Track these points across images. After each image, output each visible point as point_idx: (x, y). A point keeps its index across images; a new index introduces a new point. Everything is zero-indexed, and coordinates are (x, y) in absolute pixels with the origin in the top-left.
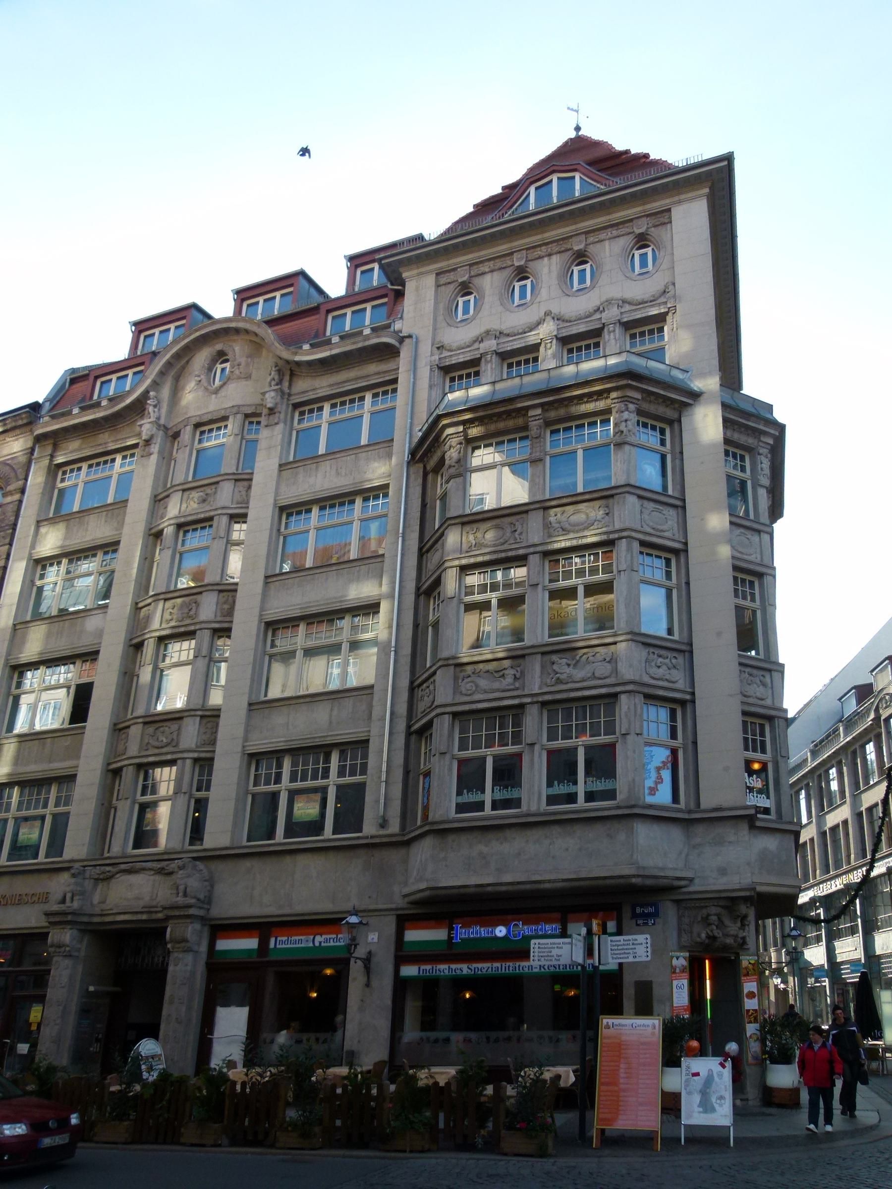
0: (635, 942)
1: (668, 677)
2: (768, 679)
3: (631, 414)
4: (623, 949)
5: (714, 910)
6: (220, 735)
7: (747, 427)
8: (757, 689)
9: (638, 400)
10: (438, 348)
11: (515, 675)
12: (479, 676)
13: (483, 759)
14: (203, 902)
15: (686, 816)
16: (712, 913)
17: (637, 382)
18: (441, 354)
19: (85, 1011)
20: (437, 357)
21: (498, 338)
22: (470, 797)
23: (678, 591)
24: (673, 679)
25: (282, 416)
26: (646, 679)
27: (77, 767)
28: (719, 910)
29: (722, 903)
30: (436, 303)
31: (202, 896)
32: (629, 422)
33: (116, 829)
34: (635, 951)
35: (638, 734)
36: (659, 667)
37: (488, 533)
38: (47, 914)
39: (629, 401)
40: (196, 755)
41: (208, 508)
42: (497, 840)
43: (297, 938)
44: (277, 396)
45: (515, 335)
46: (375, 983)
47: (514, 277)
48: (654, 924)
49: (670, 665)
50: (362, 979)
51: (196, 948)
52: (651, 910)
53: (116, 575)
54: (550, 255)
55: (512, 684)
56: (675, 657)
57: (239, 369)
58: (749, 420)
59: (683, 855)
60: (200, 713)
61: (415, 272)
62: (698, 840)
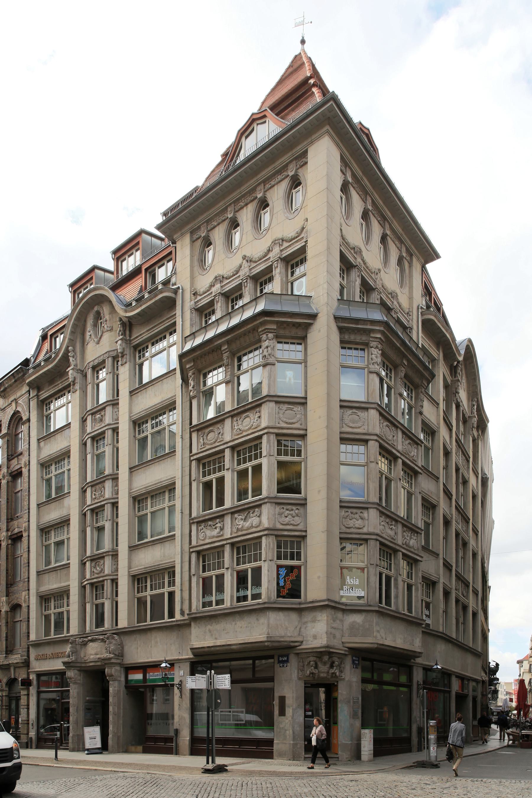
5: (312, 659)
6: (119, 567)
7: (359, 330)
8: (357, 522)
9: (275, 329)
10: (194, 294)
11: (220, 527)
14: (118, 656)
18: (196, 298)
19: (88, 709)
20: (193, 302)
21: (222, 282)
22: (242, 593)
24: (295, 524)
25: (128, 357)
27: (69, 585)
28: (315, 659)
30: (192, 256)
31: (117, 653)
32: (269, 348)
35: (271, 560)
36: (286, 517)
37: (210, 434)
39: (268, 332)
40: (111, 577)
41: (103, 425)
42: (215, 622)
43: (156, 673)
44: (123, 343)
45: (230, 278)
46: (183, 696)
47: (231, 227)
48: (286, 666)
50: (179, 694)
51: (119, 679)
52: (286, 659)
53: (71, 471)
54: (247, 205)
56: (297, 509)
57: (106, 324)
59: (298, 628)
60: (110, 553)
61: (179, 234)
62: (305, 620)
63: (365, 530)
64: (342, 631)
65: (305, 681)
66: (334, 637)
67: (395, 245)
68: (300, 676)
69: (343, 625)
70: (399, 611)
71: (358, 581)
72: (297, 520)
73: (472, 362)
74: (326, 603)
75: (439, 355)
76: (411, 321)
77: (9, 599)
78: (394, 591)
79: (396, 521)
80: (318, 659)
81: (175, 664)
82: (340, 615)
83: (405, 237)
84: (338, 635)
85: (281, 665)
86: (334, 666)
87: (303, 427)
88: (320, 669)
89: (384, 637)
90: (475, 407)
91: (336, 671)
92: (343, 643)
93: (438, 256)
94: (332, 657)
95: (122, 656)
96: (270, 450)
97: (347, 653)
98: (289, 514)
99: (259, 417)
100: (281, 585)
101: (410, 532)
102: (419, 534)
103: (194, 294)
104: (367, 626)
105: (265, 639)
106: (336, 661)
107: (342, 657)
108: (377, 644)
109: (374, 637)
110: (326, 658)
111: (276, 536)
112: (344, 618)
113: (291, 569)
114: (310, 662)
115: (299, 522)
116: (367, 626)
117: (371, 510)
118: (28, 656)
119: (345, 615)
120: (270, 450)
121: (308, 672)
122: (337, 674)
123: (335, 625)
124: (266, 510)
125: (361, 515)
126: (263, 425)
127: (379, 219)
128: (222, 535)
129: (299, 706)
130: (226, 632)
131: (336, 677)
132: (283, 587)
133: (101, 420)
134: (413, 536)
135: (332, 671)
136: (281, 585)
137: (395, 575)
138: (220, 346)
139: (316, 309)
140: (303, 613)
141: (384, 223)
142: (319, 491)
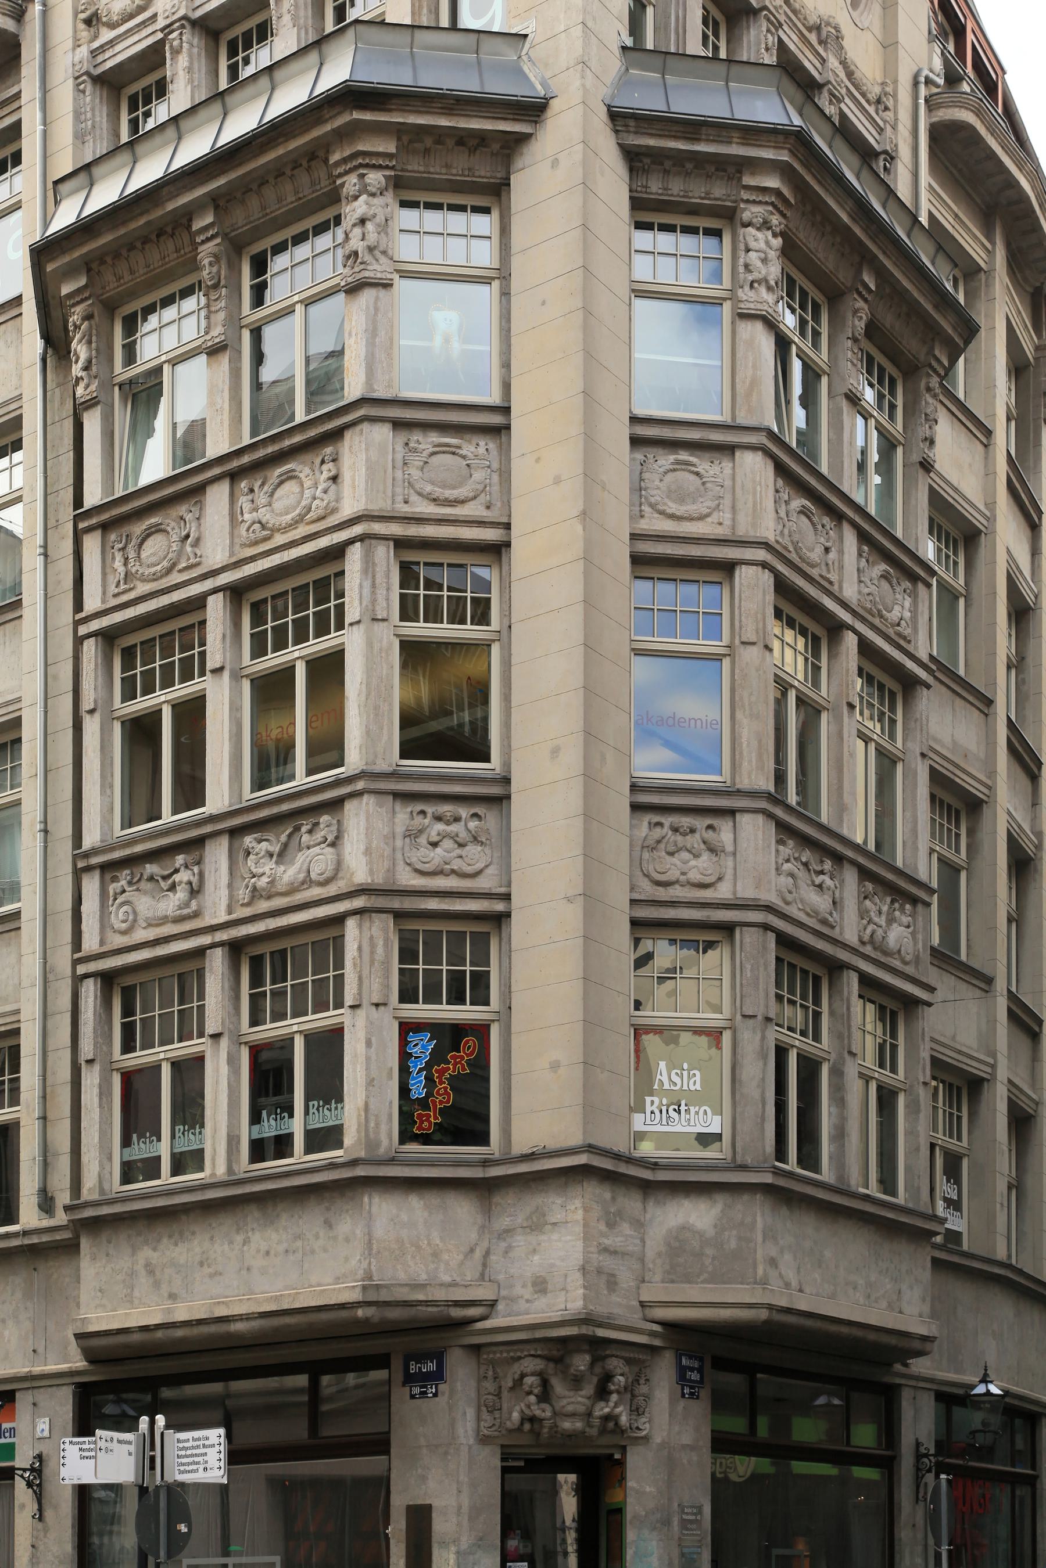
0: (207, 1443)
1: (456, 865)
3: (378, 201)
4: (192, 1456)
5: (531, 1365)
9: (389, 156)
10: (88, 22)
12: (138, 890)
13: (287, 1043)
15: (477, 1173)
16: (528, 1370)
17: (373, 109)
18: (96, 37)
20: (84, 51)
22: (269, 1128)
23: (502, 648)
26: (408, 879)
32: (370, 226)
34: (206, 1458)
35: (377, 1005)
42: (170, 1237)
46: (48, 1514)
48: (435, 1395)
49: (463, 835)
50: (32, 1507)
52: (431, 1366)
55: (187, 905)
56: (475, 815)
58: (697, 140)
59: (478, 1254)
62: (505, 1222)
63: (723, 892)
64: (642, 1260)
65: (502, 1446)
66: (612, 1283)
68: (486, 1432)
69: (643, 1241)
70: (849, 1186)
71: (698, 1078)
76: (889, 129)
78: (830, 1113)
80: (551, 1365)
81: (18, 1395)
82: (631, 1203)
84: (626, 1278)
85: (416, 1390)
86: (611, 1393)
89: (794, 1284)
91: (618, 1410)
92: (643, 1305)
94: (604, 1358)
96: (374, 601)
97: (657, 1342)
98: (443, 836)
99: (334, 479)
100: (414, 1095)
103: (88, 22)
104: (733, 1244)
106: (619, 1371)
108: (770, 1307)
109: (755, 1283)
110: (581, 1362)
111: (399, 915)
112: (648, 1216)
115: (480, 866)
116: (733, 1244)
119: (651, 1204)
120: (374, 601)
121: (516, 1415)
122: (624, 1419)
125: (710, 835)
128: (196, 915)
129: (481, 1539)
130: (211, 1270)
131: (619, 1430)
132: (423, 1103)
134: (897, 913)
135: (602, 1409)
138: (187, 214)
142: (555, 751)
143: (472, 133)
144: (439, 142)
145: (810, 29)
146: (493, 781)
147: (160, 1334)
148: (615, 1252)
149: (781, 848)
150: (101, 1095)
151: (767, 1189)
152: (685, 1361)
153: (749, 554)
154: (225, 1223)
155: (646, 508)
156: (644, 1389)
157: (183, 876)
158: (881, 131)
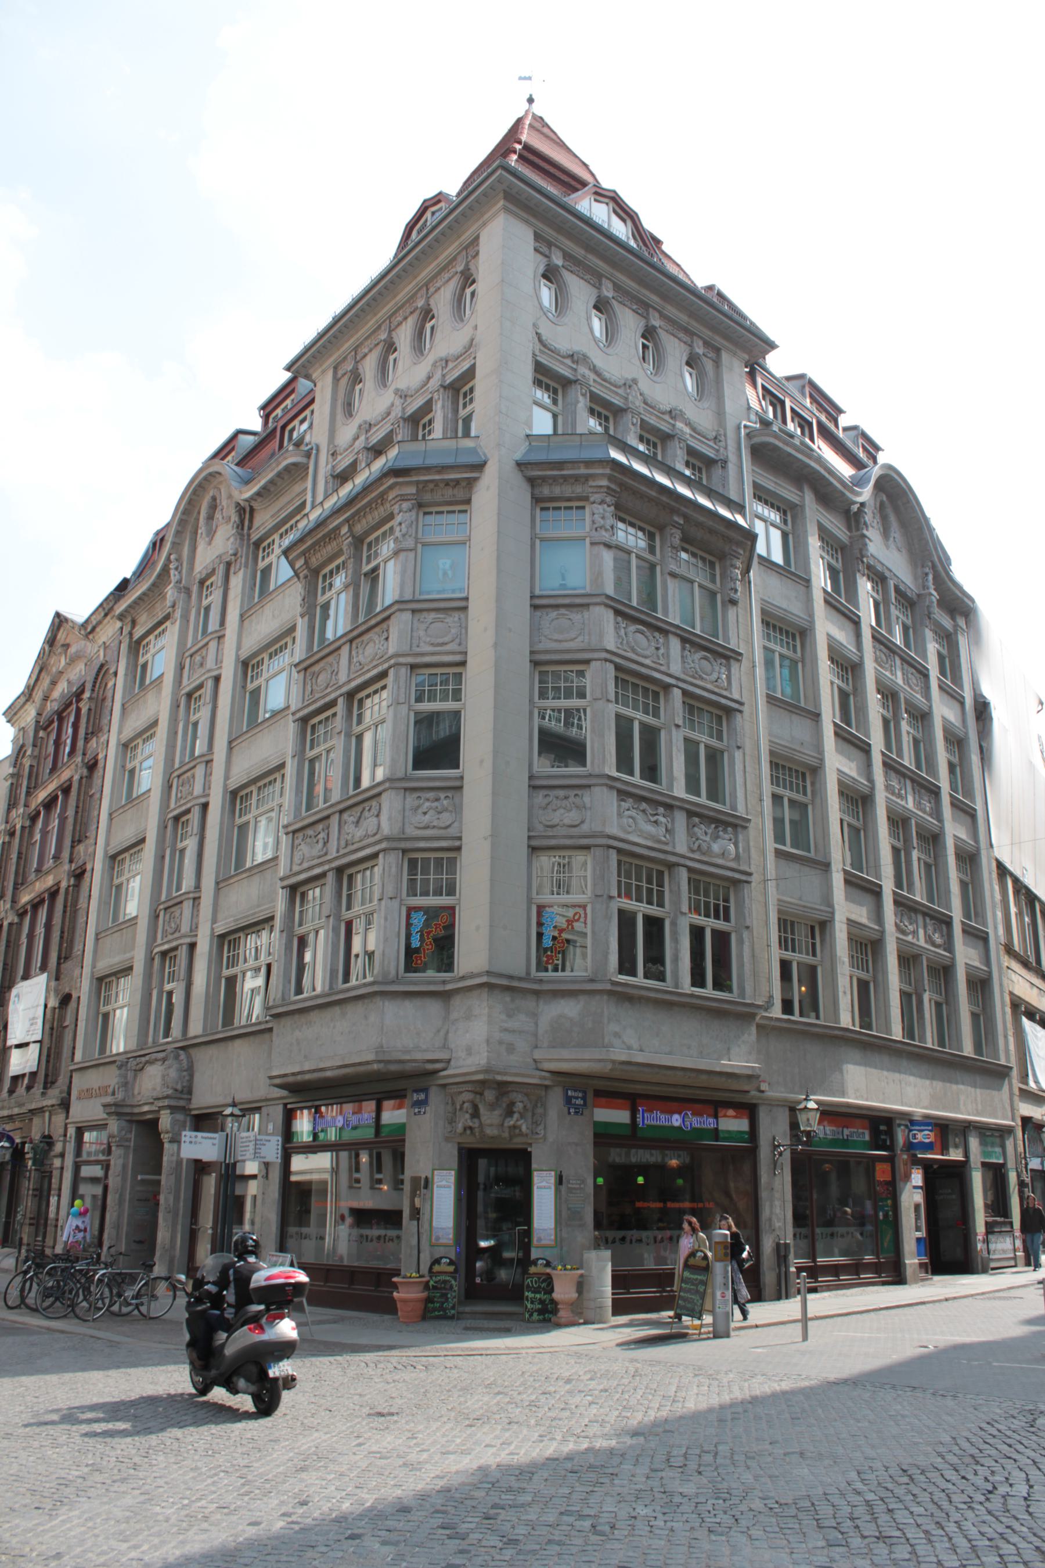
2: (587, 799)
7: (565, 478)
16: (466, 1099)
20: (330, 466)
26: (411, 831)
29: (470, 1087)
31: (179, 1087)
32: (403, 525)
33: (849, 1015)
36: (425, 813)
38: (105, 1106)
59: (442, 1033)
63: (585, 828)
64: (536, 1035)
65: (459, 1143)
66: (511, 1048)
67: (679, 339)
69: (536, 1024)
72: (446, 818)
73: (909, 501)
74: (484, 979)
75: (803, 497)
76: (722, 450)
77: (59, 985)
79: (669, 807)
82: (529, 1003)
83: (695, 326)
85: (417, 1110)
87: (461, 649)
88: (483, 1119)
89: (636, 1046)
90: (930, 577)
91: (519, 1123)
92: (535, 1061)
93: (772, 346)
94: (508, 1092)
95: (190, 1092)
96: (398, 695)
97: (547, 1083)
98: (430, 808)
99: (387, 639)
100: (413, 946)
101: (713, 826)
102: (739, 829)
103: (333, 455)
105: (370, 1057)
107: (536, 1093)
108: (613, 1062)
111: (404, 851)
113: (431, 913)
114: (464, 1102)
115: (448, 823)
117: (596, 790)
118: (69, 1094)
120: (398, 695)
122: (524, 1128)
123: (510, 1024)
124: (390, 804)
125: (577, 800)
126: (391, 651)
127: (635, 307)
128: (326, 854)
133: (202, 665)
134: (721, 833)
136: (413, 946)
137: (672, 915)
138: (338, 528)
139: (485, 455)
140: (452, 1002)
141: (647, 310)
142: (482, 762)
143: (452, 480)
144: (436, 485)
145: (663, 413)
146: (456, 778)
147: (299, 1078)
148: (514, 1031)
149: (623, 803)
150: (286, 949)
151: (610, 993)
152: (570, 1093)
153: (596, 655)
154: (328, 1014)
155: (543, 638)
156: (540, 1110)
157: (321, 836)
158: (718, 451)
